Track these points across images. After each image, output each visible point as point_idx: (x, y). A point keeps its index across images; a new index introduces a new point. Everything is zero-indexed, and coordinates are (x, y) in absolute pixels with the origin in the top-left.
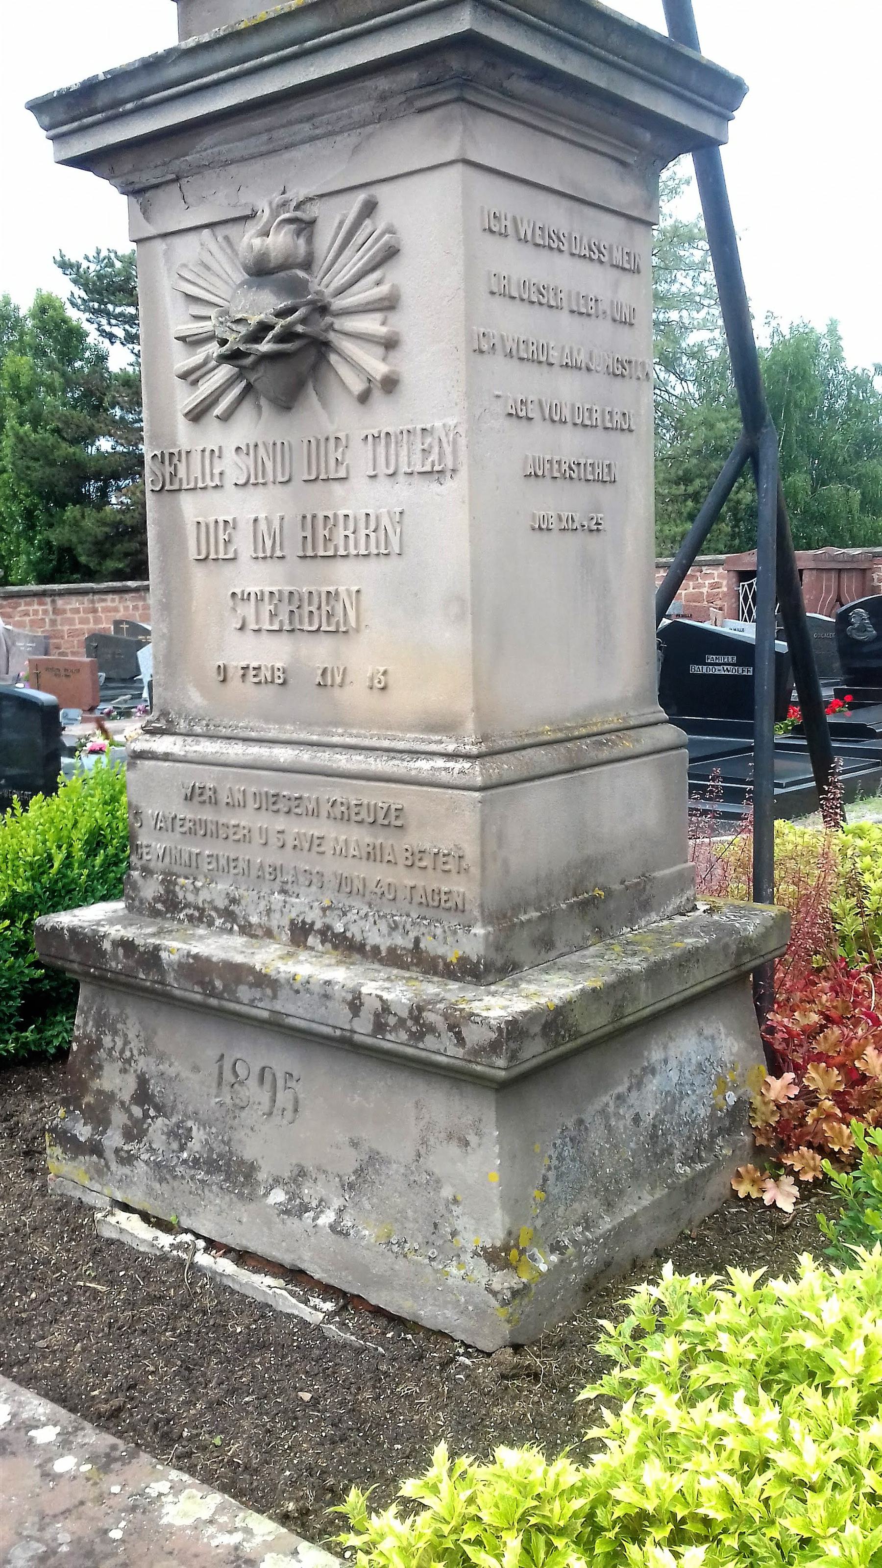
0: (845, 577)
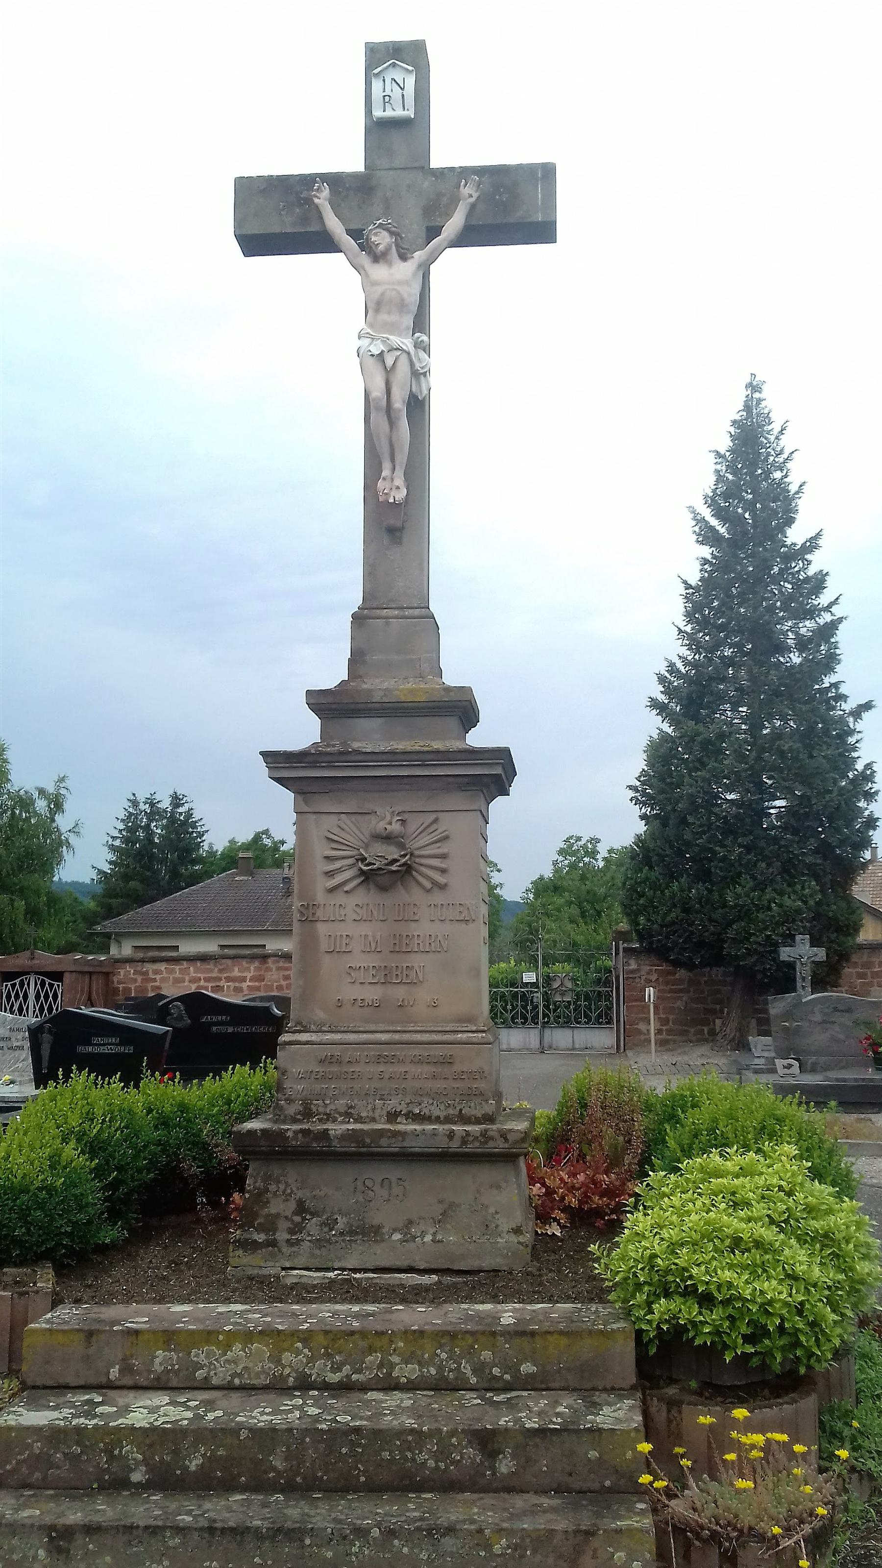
0: (94, 977)
